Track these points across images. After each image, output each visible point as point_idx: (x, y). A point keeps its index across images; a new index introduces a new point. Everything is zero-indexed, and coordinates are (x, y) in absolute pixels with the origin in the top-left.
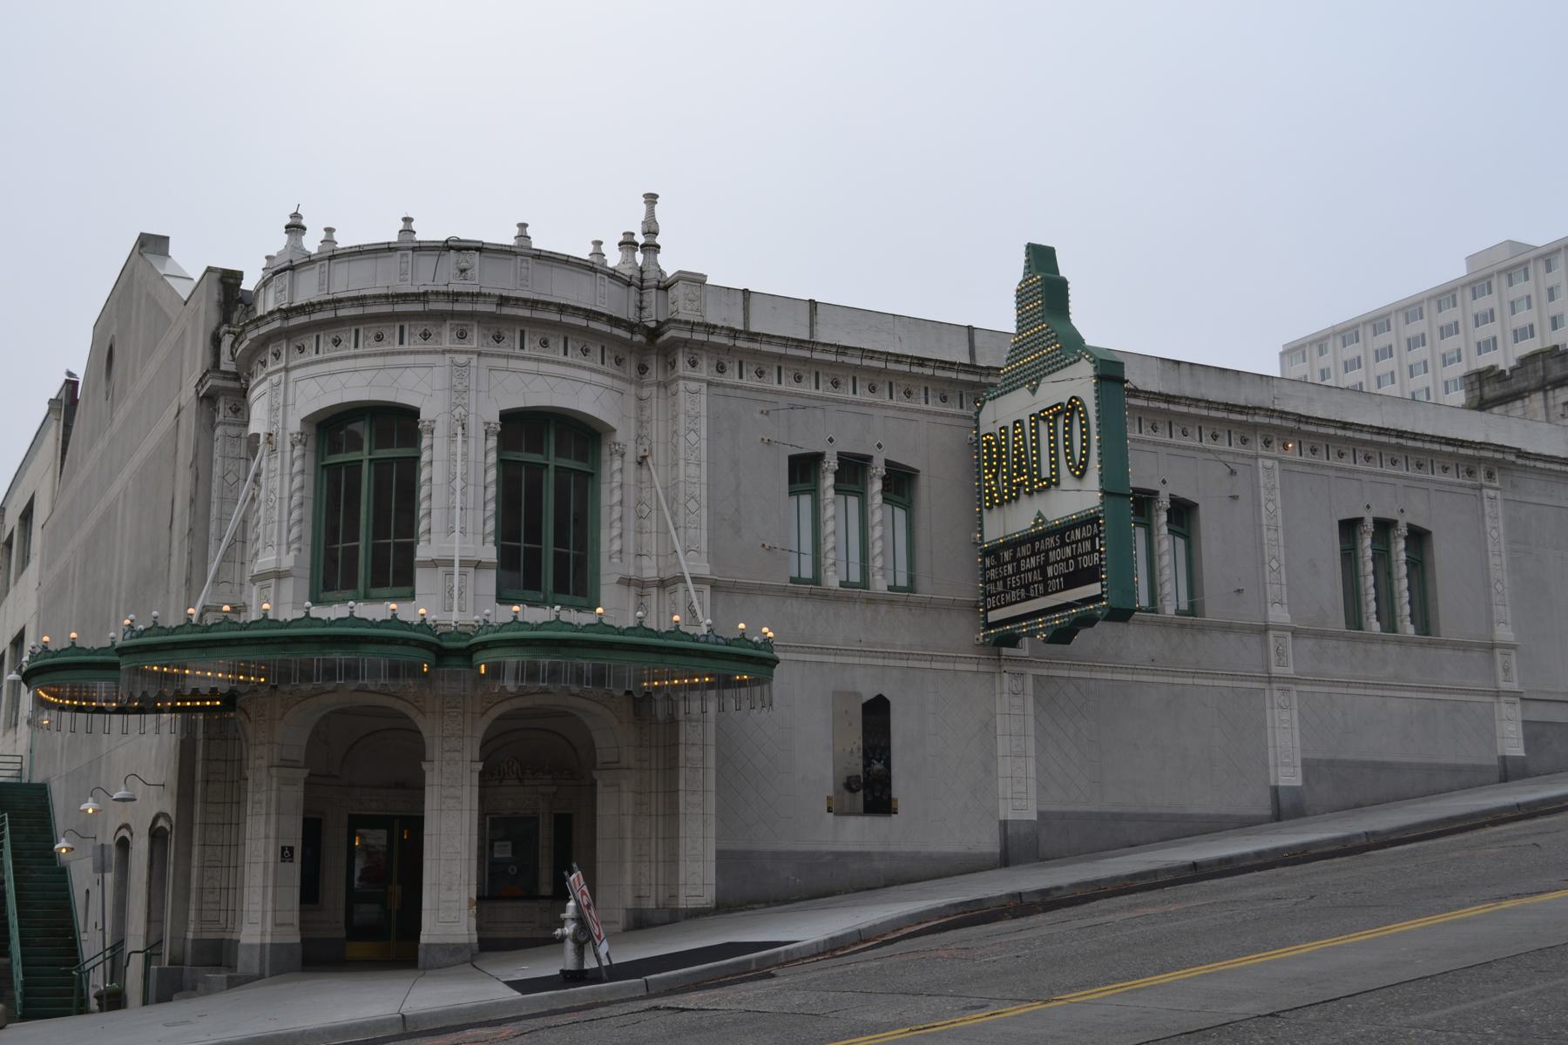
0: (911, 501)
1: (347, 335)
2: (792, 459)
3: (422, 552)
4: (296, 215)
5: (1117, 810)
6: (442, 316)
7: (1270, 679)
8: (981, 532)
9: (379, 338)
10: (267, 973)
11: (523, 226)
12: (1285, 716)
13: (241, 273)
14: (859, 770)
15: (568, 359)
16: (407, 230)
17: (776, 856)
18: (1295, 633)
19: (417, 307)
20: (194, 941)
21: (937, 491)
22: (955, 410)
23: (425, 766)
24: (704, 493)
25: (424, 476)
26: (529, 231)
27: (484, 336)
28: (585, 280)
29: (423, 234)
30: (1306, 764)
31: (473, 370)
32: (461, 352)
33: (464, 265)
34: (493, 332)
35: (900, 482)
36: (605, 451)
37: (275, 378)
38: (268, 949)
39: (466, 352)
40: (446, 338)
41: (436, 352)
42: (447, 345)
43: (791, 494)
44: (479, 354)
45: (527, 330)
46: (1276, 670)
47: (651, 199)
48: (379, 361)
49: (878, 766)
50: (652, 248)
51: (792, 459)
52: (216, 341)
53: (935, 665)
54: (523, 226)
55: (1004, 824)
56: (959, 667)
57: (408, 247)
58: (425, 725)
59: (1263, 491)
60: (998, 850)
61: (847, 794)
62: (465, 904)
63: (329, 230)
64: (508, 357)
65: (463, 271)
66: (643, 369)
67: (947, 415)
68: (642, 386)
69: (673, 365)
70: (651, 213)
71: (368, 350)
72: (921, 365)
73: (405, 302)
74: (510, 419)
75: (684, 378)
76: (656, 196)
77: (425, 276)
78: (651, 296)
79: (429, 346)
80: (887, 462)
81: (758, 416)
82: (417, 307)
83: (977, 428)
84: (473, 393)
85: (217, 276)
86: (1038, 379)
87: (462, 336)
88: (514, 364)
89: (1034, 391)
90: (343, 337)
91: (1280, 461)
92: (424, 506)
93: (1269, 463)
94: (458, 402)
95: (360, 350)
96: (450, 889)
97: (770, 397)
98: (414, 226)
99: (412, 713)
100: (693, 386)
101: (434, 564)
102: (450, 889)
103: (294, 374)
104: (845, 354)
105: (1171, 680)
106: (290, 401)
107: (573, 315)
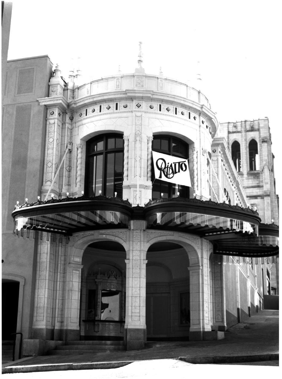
23: (126, 261)
37: (139, 114)
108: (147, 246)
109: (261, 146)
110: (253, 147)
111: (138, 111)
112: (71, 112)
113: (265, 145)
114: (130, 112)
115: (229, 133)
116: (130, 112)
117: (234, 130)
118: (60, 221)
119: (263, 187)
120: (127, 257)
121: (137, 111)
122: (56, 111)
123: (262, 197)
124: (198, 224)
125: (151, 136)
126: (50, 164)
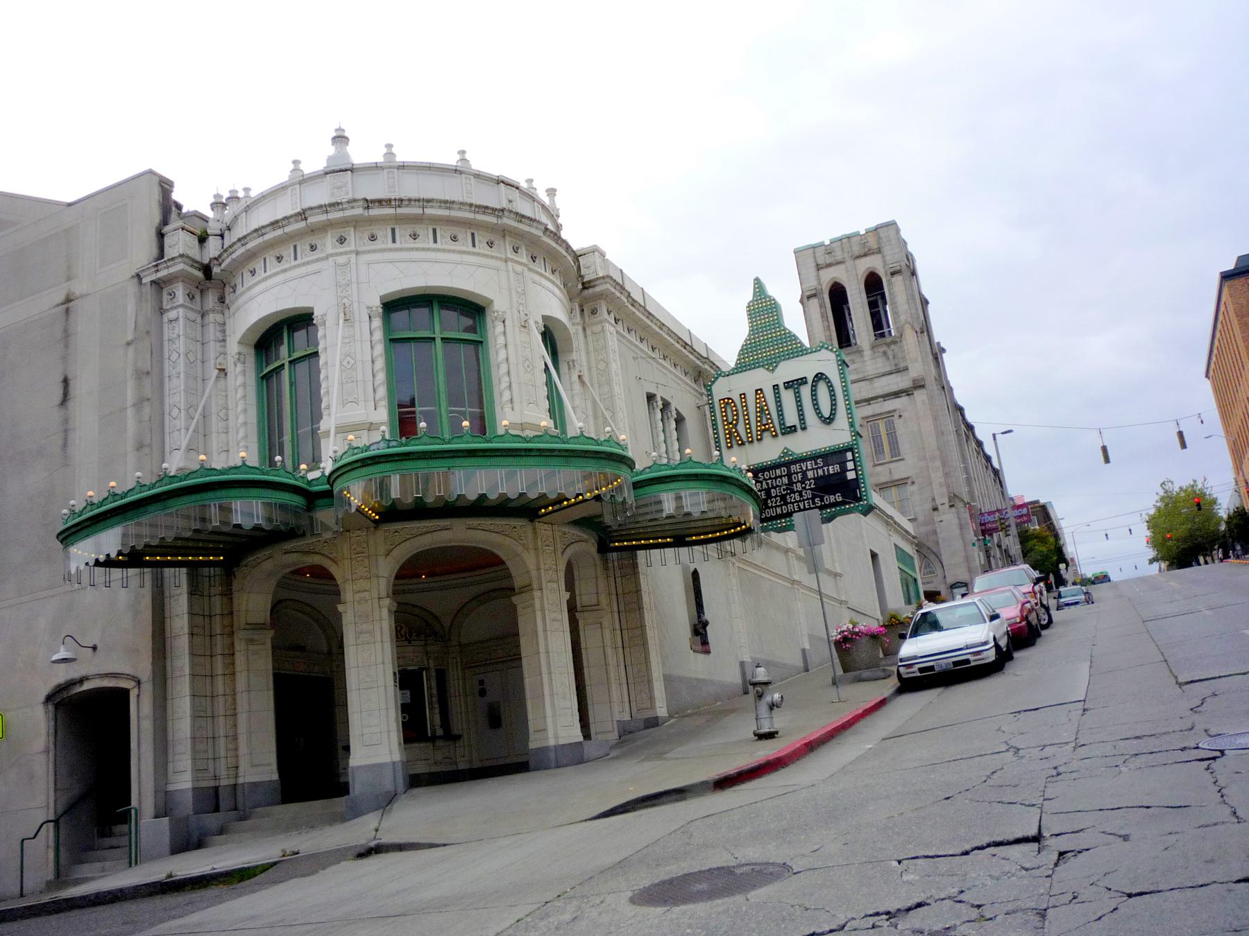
1: (288, 252)
6: (355, 223)
15: (476, 250)
16: (390, 154)
19: (492, 219)
20: (194, 789)
23: (340, 608)
27: (361, 238)
28: (456, 180)
31: (353, 267)
32: (341, 254)
33: (511, 198)
34: (410, 231)
36: (489, 320)
37: (341, 260)
38: (399, 767)
39: (346, 253)
40: (328, 243)
41: (322, 259)
42: (330, 250)
52: (161, 236)
54: (389, 146)
63: (296, 162)
69: (594, 312)
73: (484, 213)
74: (392, 306)
79: (317, 254)
82: (492, 219)
84: (354, 286)
86: (778, 363)
87: (342, 240)
88: (466, 258)
90: (284, 253)
92: (324, 385)
94: (342, 293)
95: (299, 261)
98: (394, 150)
99: (326, 563)
103: (364, 258)
108: (386, 568)
109: (890, 284)
110: (873, 284)
111: (341, 254)
112: (212, 281)
113: (898, 279)
114: (501, 259)
115: (819, 268)
116: (501, 259)
117: (829, 260)
118: (220, 542)
119: (906, 369)
120: (518, 582)
121: (337, 254)
122: (180, 291)
123: (907, 392)
124: (522, 495)
125: (376, 303)
126: (175, 412)
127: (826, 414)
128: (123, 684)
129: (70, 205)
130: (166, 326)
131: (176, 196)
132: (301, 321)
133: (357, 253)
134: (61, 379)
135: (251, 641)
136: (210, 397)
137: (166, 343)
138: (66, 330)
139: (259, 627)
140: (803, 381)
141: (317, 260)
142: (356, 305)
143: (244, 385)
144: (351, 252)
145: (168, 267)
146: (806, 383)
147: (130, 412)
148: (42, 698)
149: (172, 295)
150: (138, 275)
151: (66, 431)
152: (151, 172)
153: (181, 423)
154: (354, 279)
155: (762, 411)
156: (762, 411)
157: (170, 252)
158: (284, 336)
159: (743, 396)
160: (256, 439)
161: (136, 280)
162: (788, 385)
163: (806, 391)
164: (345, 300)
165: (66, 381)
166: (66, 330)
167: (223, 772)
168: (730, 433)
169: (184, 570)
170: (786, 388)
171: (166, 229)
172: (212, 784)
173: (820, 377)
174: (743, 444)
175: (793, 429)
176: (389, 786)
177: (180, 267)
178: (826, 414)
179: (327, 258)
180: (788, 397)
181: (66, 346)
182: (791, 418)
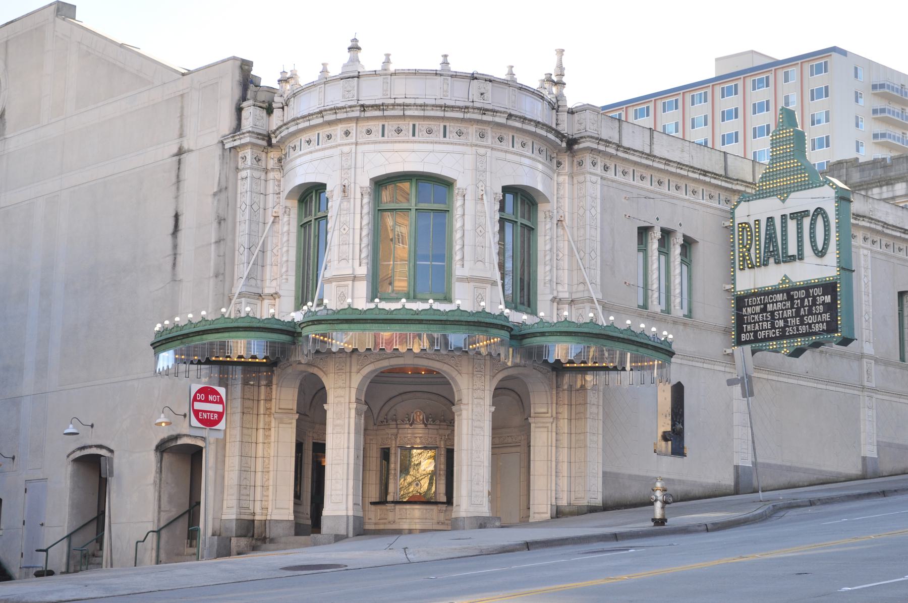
0: (691, 261)
2: (639, 228)
3: (458, 271)
4: (355, 40)
5: (789, 464)
7: (863, 388)
8: (734, 284)
9: (430, 132)
10: (351, 534)
11: (445, 56)
12: (870, 413)
13: (252, 63)
14: (669, 429)
17: (631, 477)
18: (876, 361)
19: (460, 115)
21: (708, 255)
22: (716, 205)
23: (326, 406)
24: (599, 248)
25: (458, 224)
26: (449, 60)
29: (455, 67)
30: (879, 445)
34: (498, 135)
35: (688, 244)
37: (346, 149)
42: (339, 141)
43: (639, 250)
44: (492, 149)
45: (447, 124)
46: (866, 384)
47: (561, 52)
48: (430, 147)
49: (680, 426)
50: (560, 84)
51: (639, 228)
52: (239, 110)
53: (705, 366)
54: (445, 56)
55: (737, 467)
56: (716, 368)
57: (444, 74)
58: (329, 382)
59: (566, 267)
60: (733, 484)
61: (663, 443)
62: (486, 493)
64: (506, 152)
65: (482, 94)
66: (559, 164)
67: (710, 207)
68: (558, 175)
70: (560, 60)
71: (421, 139)
72: (705, 175)
74: (380, 183)
75: (590, 173)
76: (563, 50)
77: (458, 94)
78: (564, 116)
80: (684, 236)
81: (623, 200)
82: (460, 115)
83: (733, 218)
85: (239, 63)
86: (789, 193)
88: (510, 157)
89: (783, 201)
91: (871, 250)
93: (866, 252)
96: (478, 484)
97: (628, 189)
100: (594, 178)
101: (468, 280)
102: (478, 484)
103: (361, 148)
104: (669, 165)
105: (815, 385)
106: (359, 165)
107: (542, 128)
122: (248, 153)
125: (367, 183)
127: (820, 248)
128: (200, 443)
129: (183, 74)
130: (239, 182)
131: (255, 72)
132: (320, 188)
133: (356, 144)
134: (174, 214)
135: (281, 422)
136: (267, 237)
137: (239, 195)
138: (178, 176)
139: (287, 411)
140: (805, 213)
141: (331, 148)
142: (352, 185)
143: (288, 232)
144: (352, 144)
145: (240, 139)
146: (808, 216)
147: (213, 247)
148: (154, 447)
149: (244, 158)
150: (222, 142)
151: (175, 254)
152: (234, 58)
153: (244, 258)
154: (353, 166)
155: (771, 238)
156: (771, 238)
157: (247, 125)
158: (311, 195)
159: (758, 221)
160: (294, 274)
161: (220, 145)
162: (793, 216)
163: (807, 222)
164: (346, 182)
165: (177, 217)
166: (178, 176)
167: (258, 510)
168: (744, 257)
169: (239, 368)
170: (792, 218)
171: (244, 104)
172: (250, 518)
173: (819, 211)
174: (753, 267)
175: (792, 259)
176: (343, 532)
177: (247, 139)
178: (820, 248)
179: (336, 146)
180: (792, 225)
181: (178, 189)
182: (792, 250)
